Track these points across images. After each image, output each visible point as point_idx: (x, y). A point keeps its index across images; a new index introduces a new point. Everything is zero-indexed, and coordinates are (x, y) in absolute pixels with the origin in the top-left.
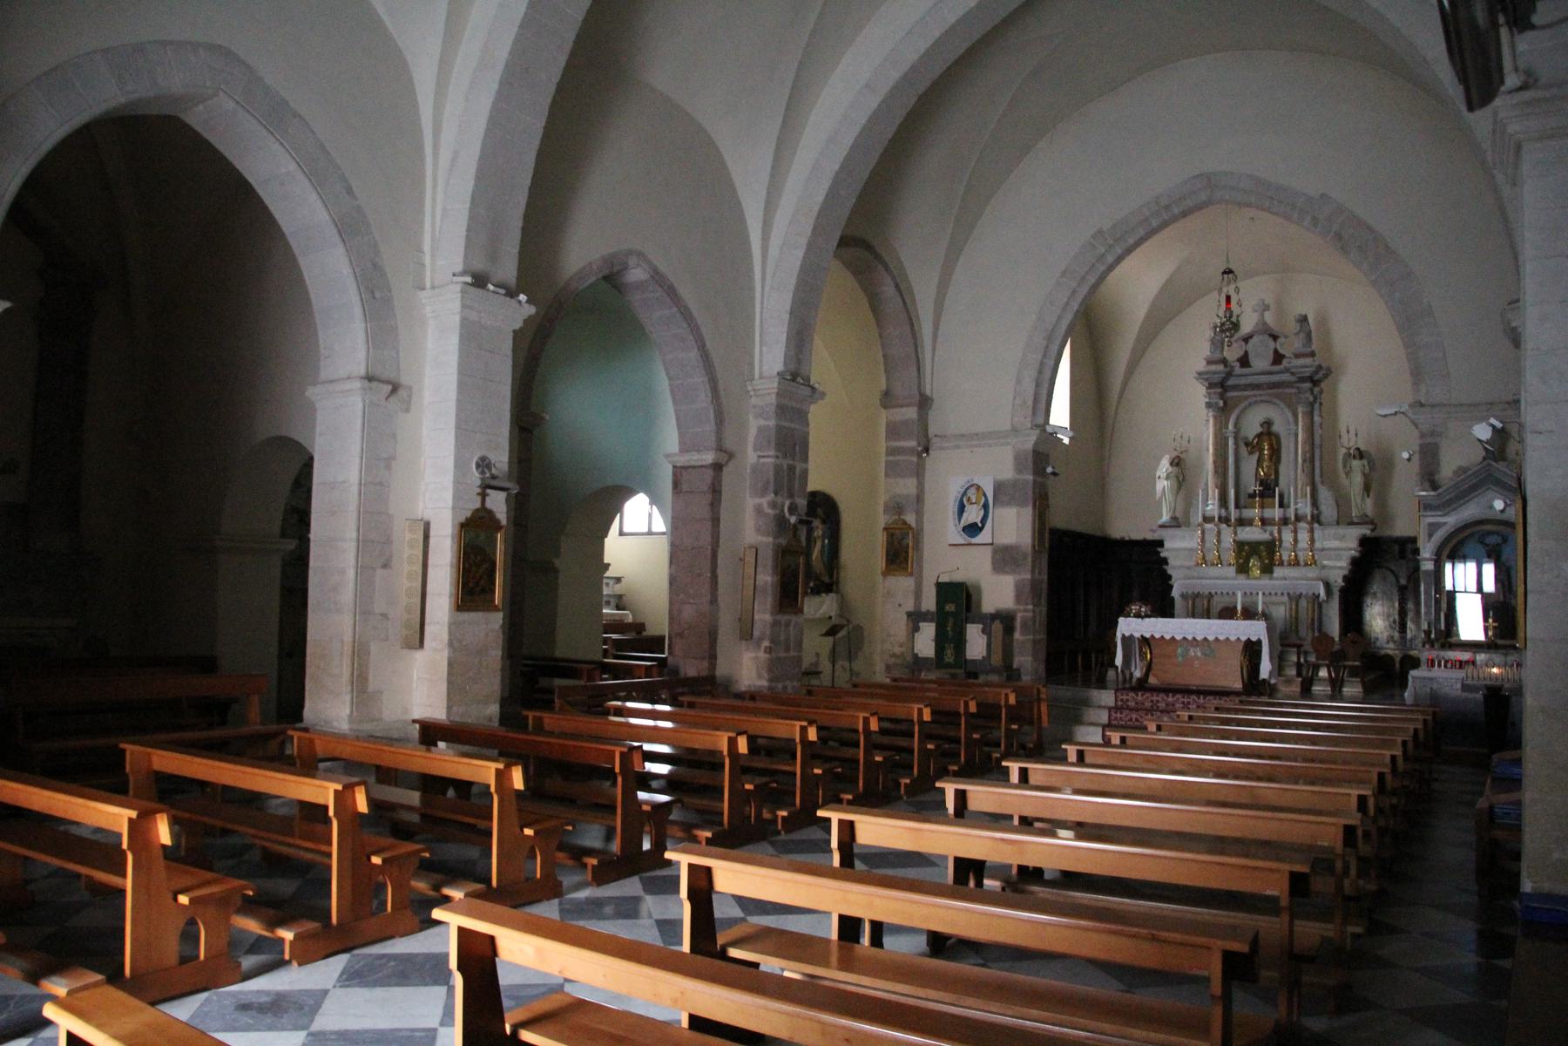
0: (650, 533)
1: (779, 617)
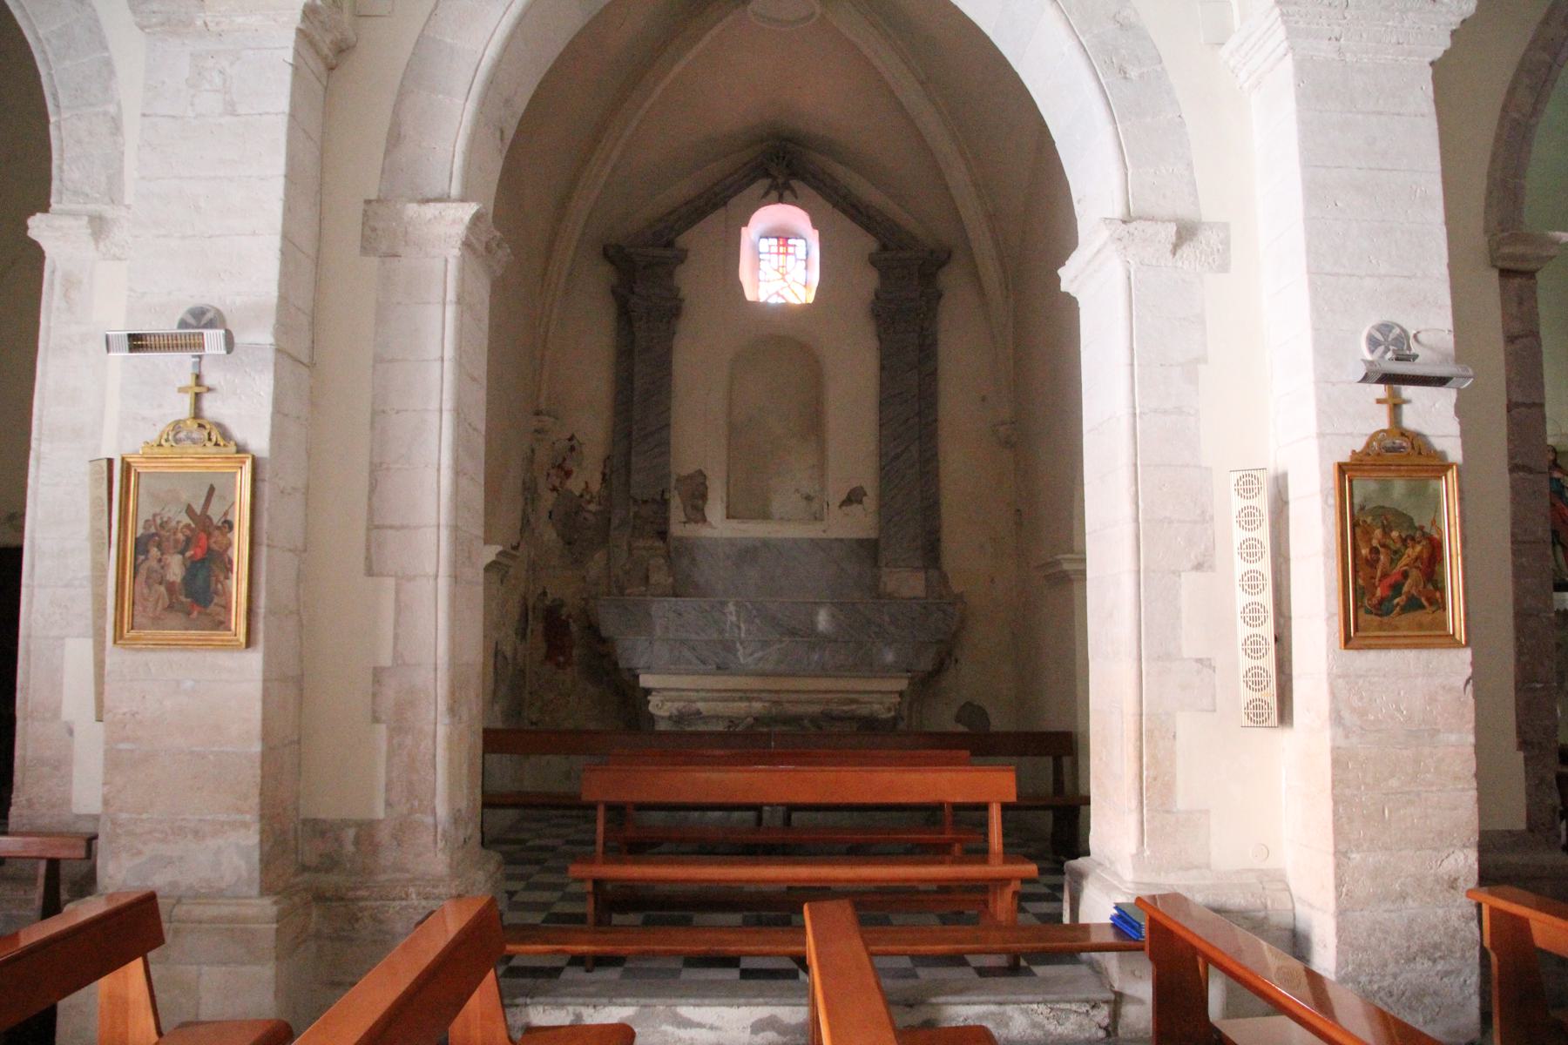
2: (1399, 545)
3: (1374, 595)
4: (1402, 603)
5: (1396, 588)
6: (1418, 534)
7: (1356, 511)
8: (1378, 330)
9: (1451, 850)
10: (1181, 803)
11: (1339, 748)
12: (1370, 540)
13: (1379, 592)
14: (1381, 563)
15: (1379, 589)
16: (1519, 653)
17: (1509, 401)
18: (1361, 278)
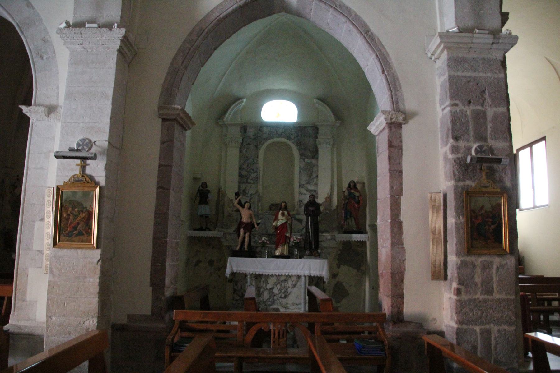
0: (535, 207)
1: (468, 259)
2: (77, 213)
3: (67, 230)
4: (76, 233)
5: (75, 228)
6: (85, 210)
7: (63, 202)
8: (81, 141)
9: (88, 318)
10: (28, 298)
11: (51, 281)
12: (67, 211)
13: (69, 229)
14: (70, 219)
15: (69, 228)
16: (153, 252)
18: (79, 123)
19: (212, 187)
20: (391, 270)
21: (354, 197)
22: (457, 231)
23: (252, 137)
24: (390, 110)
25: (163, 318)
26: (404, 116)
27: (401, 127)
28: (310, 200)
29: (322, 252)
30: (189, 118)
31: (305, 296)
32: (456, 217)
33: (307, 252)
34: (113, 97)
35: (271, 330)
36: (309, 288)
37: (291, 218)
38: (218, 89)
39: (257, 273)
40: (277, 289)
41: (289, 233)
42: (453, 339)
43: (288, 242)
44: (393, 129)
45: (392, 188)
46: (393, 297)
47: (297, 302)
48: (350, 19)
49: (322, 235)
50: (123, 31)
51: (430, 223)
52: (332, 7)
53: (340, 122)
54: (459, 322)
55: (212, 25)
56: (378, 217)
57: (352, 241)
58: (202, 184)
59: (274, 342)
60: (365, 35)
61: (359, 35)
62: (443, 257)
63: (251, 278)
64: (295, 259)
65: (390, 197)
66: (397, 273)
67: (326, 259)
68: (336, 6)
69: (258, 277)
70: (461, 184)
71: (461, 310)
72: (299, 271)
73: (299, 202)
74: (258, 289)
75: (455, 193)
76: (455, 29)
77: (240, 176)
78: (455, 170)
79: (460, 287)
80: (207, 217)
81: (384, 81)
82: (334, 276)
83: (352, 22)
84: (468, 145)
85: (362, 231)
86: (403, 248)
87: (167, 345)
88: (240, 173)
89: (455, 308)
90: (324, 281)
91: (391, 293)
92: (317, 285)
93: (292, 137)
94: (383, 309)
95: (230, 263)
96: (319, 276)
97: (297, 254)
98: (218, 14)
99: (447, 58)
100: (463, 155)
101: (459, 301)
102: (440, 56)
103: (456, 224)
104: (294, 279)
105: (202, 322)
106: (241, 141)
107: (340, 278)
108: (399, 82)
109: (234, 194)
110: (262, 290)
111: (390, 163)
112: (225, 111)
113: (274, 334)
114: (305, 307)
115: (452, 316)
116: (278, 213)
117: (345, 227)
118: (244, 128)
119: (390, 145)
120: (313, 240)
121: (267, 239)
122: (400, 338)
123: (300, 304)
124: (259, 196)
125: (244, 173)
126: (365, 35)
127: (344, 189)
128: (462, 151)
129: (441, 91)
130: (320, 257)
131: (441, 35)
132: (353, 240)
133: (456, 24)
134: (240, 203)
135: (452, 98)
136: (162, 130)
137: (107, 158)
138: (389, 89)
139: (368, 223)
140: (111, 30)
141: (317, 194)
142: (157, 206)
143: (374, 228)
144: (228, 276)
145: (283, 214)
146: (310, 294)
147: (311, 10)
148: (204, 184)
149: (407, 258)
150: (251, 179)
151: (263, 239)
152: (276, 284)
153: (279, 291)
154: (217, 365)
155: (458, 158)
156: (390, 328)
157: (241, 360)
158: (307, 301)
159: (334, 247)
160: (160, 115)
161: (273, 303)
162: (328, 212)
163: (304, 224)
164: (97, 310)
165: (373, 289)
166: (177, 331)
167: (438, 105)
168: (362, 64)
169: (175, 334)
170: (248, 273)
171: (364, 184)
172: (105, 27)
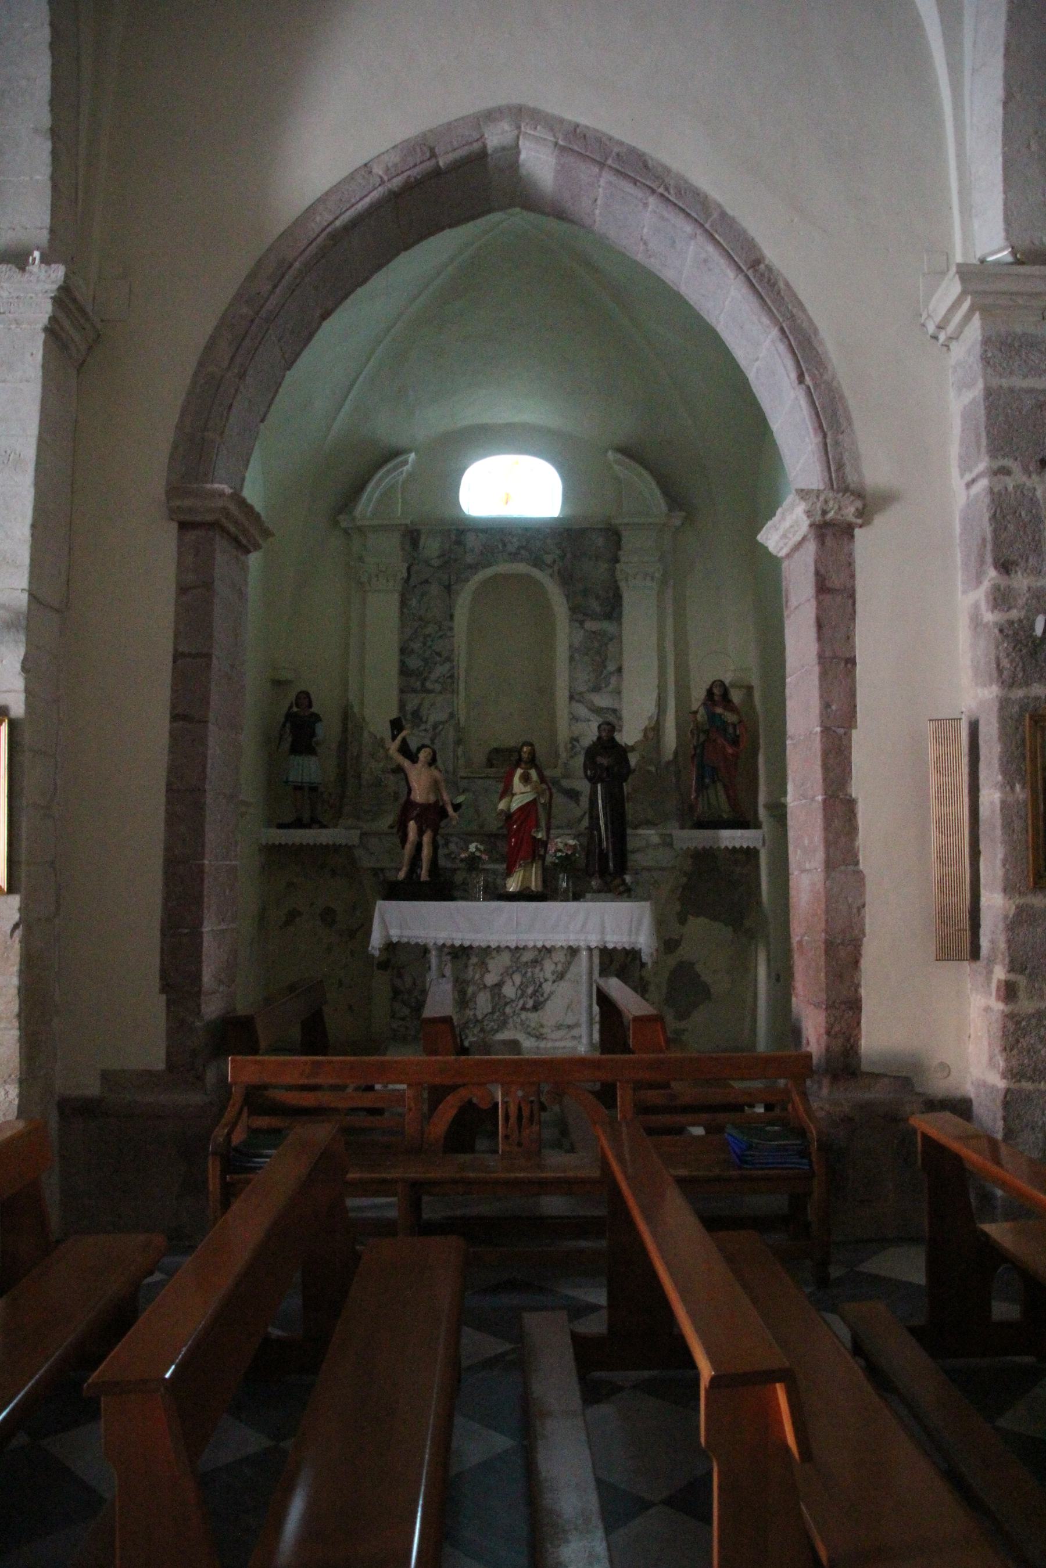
16: (167, 899)
17: (176, 650)
19: (325, 703)
20: (827, 933)
21: (722, 727)
22: (1007, 825)
23: (436, 563)
24: (822, 487)
25: (200, 1078)
26: (859, 504)
27: (852, 536)
28: (599, 738)
29: (637, 883)
30: (257, 517)
31: (590, 1006)
32: (1003, 786)
33: (595, 883)
34: (38, 464)
35: (497, 1104)
36: (602, 982)
37: (549, 789)
38: (336, 425)
39: (457, 943)
40: (514, 985)
41: (544, 833)
42: (995, 1120)
43: (540, 856)
44: (829, 542)
45: (826, 705)
46: (830, 1006)
47: (570, 1021)
48: (707, 226)
49: (637, 835)
50: (58, 272)
51: (933, 802)
52: (653, 191)
53: (684, 514)
54: (1012, 1074)
55: (313, 248)
56: (790, 788)
57: (719, 847)
58: (298, 697)
59: (506, 1137)
60: (750, 273)
61: (731, 274)
62: (968, 902)
63: (439, 956)
64: (562, 901)
65: (822, 732)
66: (842, 944)
67: (645, 900)
68: (667, 189)
69: (460, 953)
70: (1019, 693)
71: (1018, 1041)
72: (572, 937)
73: (571, 743)
74: (461, 986)
75: (1003, 720)
76: (1005, 255)
77: (404, 671)
78: (1002, 655)
79: (1012, 977)
80: (313, 789)
81: (803, 402)
82: (668, 944)
83: (711, 235)
84: (1039, 584)
85: (744, 821)
86: (859, 873)
87: (214, 1154)
88: (402, 663)
89: (1001, 1034)
90: (644, 961)
91: (825, 997)
92: (623, 975)
93: (548, 559)
94: (804, 1041)
95: (383, 921)
96: (628, 948)
97: (567, 889)
98: (331, 218)
99: (980, 338)
100: (1023, 614)
101: (1010, 1016)
102: (961, 332)
103: (1003, 803)
104: (560, 957)
105: (303, 1088)
106: (405, 575)
107: (685, 952)
108: (846, 410)
109: (388, 725)
110: (470, 990)
111: (820, 638)
112: (358, 489)
113: (507, 1118)
114: (591, 1035)
115: (991, 1058)
116: (511, 775)
117: (700, 809)
118: (412, 537)
119: (822, 587)
120: (610, 848)
121: (482, 847)
122: (851, 1119)
123: (577, 1025)
124: (458, 728)
125: (413, 663)
126: (750, 273)
127: (695, 705)
128: (1021, 602)
129: (963, 431)
130: (629, 897)
131: (966, 273)
132: (723, 846)
133: (1007, 239)
134: (405, 750)
135: (995, 450)
136: (180, 554)
137: (27, 640)
138: (816, 425)
139: (762, 799)
140: (22, 269)
141: (620, 718)
142: (173, 770)
143: (779, 812)
144: (377, 953)
145: (526, 779)
146: (604, 1000)
147: (596, 200)
148: (304, 698)
149: (868, 898)
150: (436, 681)
151: (472, 848)
152: (508, 973)
153: (519, 992)
154: (350, 1202)
155: (1011, 623)
156: (825, 1091)
157: (416, 1190)
158: (597, 1018)
159: (670, 865)
160: (172, 513)
161: (503, 1025)
162: (653, 769)
163: (584, 801)
164: (16, 1061)
165: (778, 980)
166: (240, 1113)
167: (955, 472)
168: (740, 354)
169: (234, 1125)
170: (431, 944)
171: (750, 689)
172: (8, 262)
